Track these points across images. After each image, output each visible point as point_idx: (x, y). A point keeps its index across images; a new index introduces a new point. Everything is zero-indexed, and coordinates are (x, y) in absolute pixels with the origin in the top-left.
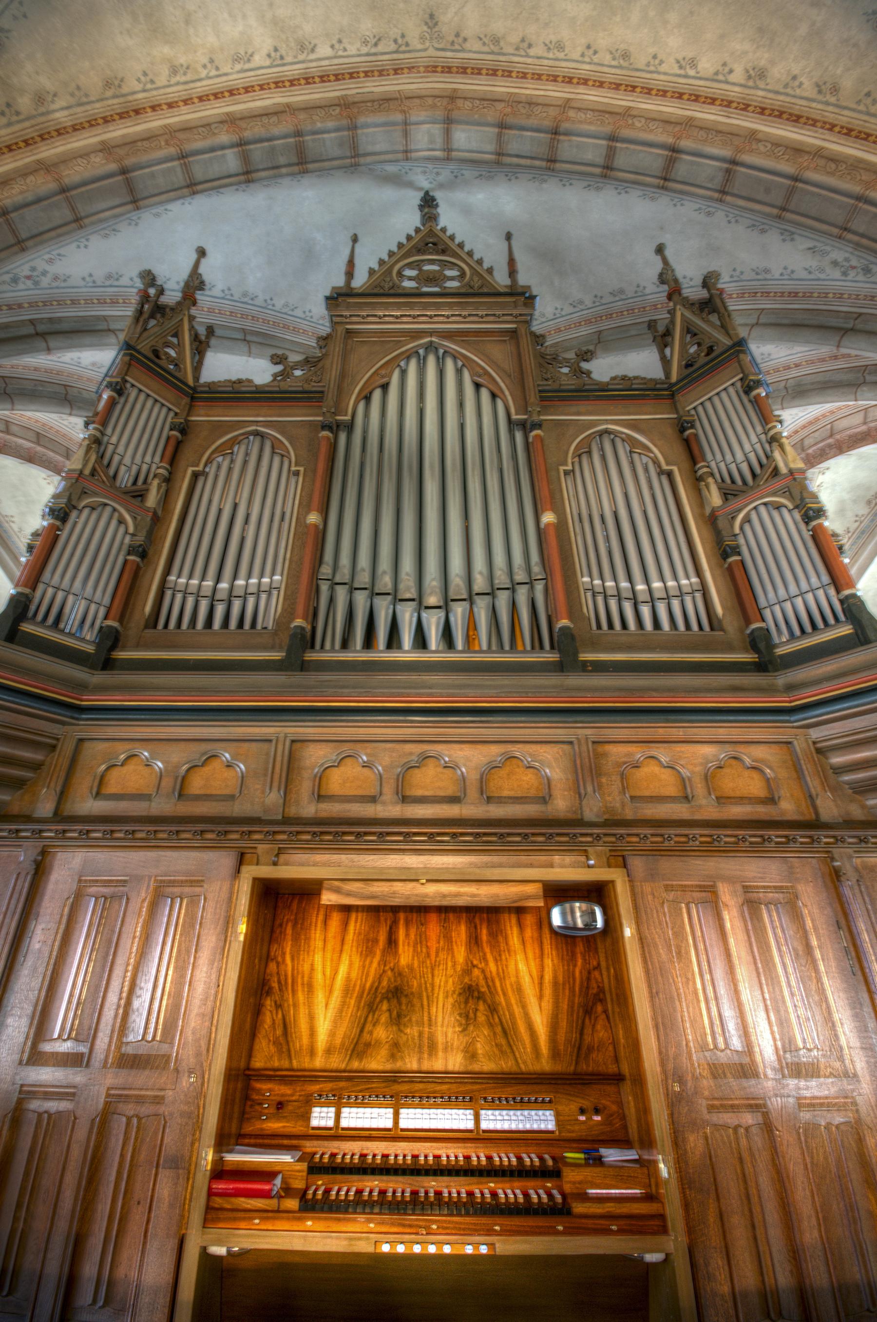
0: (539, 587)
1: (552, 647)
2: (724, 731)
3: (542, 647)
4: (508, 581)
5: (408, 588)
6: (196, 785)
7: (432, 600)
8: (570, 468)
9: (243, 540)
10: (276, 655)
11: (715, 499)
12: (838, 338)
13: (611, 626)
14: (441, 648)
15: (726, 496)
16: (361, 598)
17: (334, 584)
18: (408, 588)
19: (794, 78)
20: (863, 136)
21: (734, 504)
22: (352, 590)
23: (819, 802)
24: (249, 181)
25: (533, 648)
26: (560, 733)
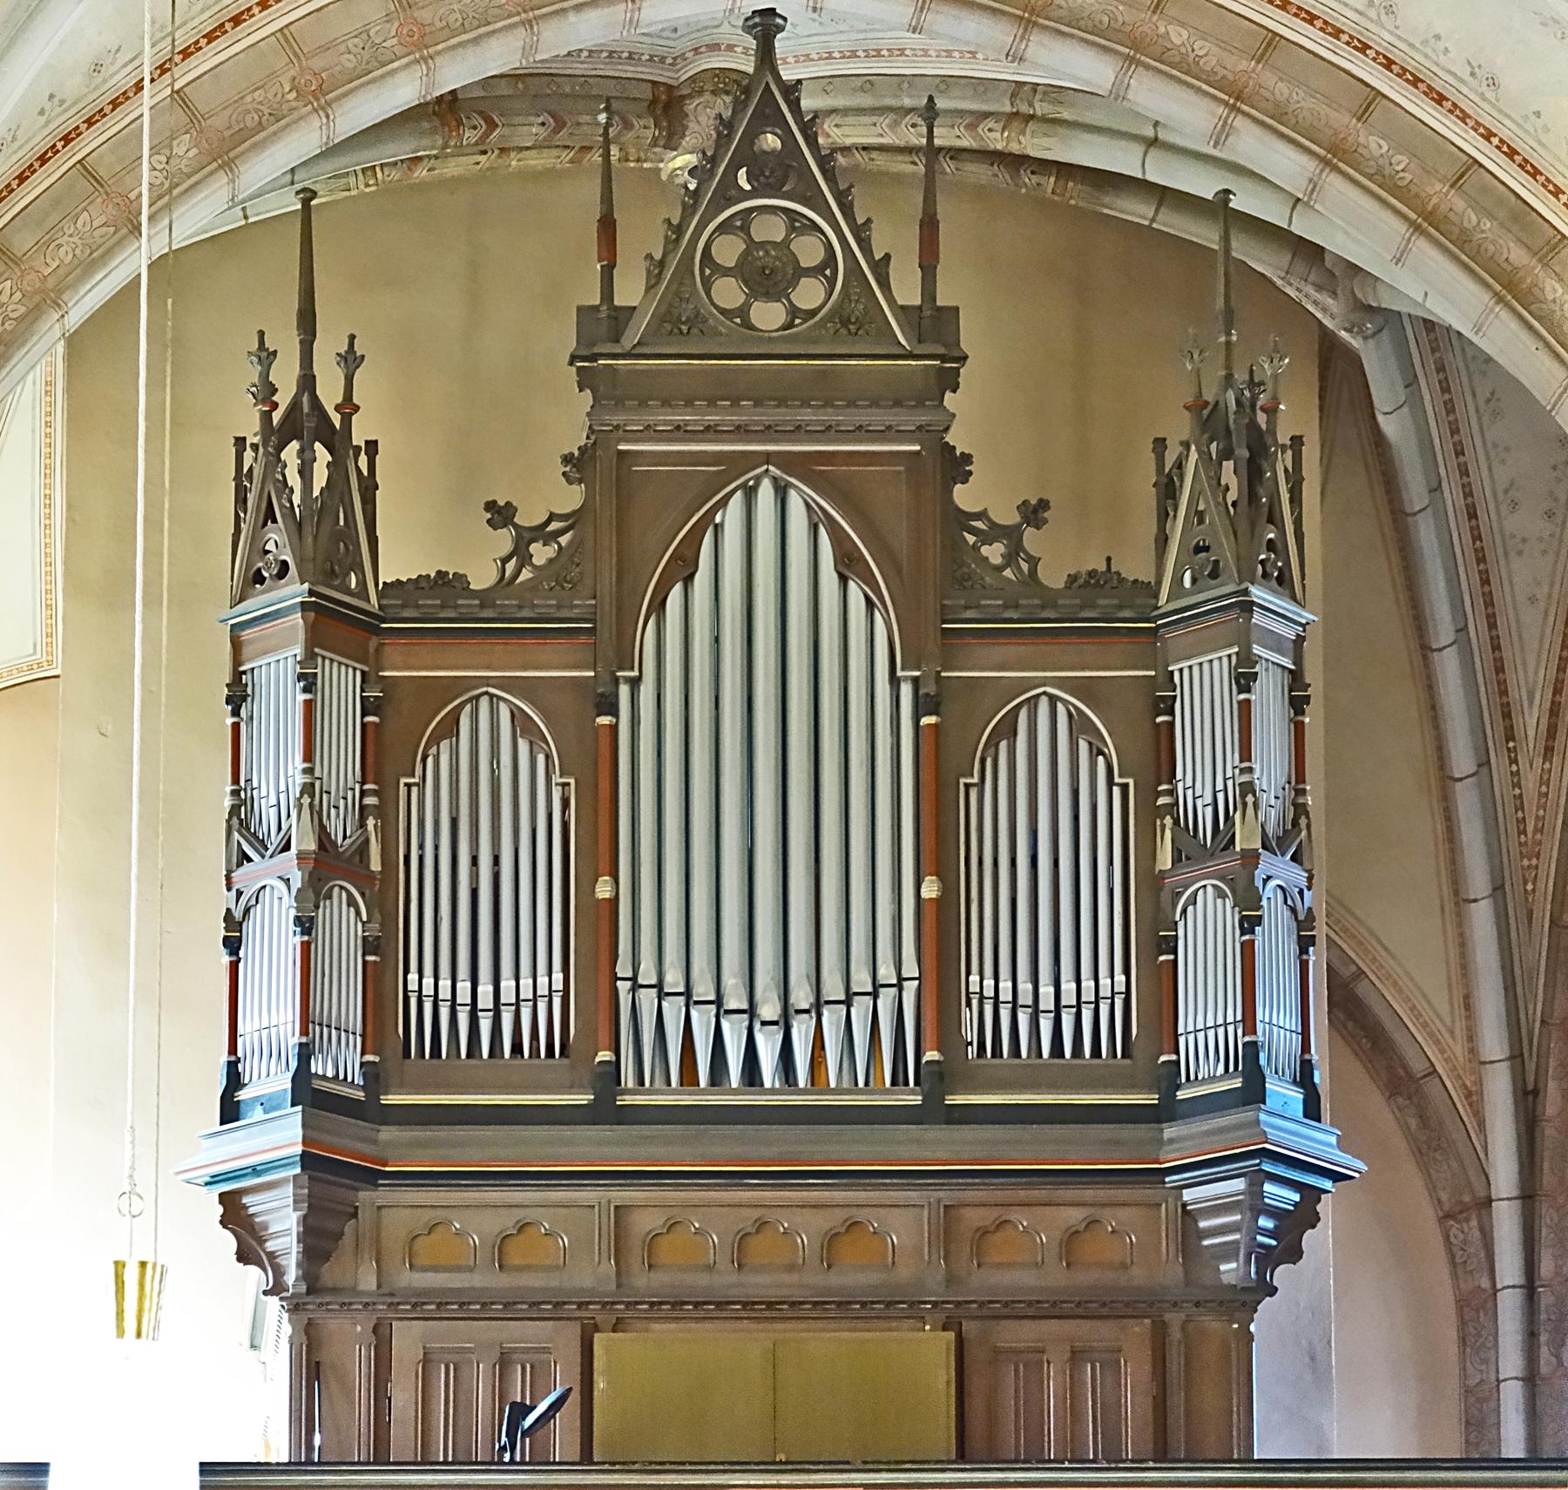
0: (910, 988)
1: (917, 1083)
2: (1089, 1194)
3: (906, 1083)
4: (870, 981)
5: (674, 981)
6: (514, 1258)
7: (732, 1004)
8: (975, 780)
9: (474, 893)
10: (583, 1099)
11: (1165, 860)
12: (1410, 519)
13: (997, 1052)
14: (777, 1085)
15: (1177, 859)
16: (673, 1010)
17: (636, 986)
18: (674, 981)
19: (1437, 37)
20: (1551, 187)
21: (1186, 873)
22: (662, 995)
23: (1505, 523)
24: (1468, 1423)
25: (894, 1083)
26: (913, 1196)
